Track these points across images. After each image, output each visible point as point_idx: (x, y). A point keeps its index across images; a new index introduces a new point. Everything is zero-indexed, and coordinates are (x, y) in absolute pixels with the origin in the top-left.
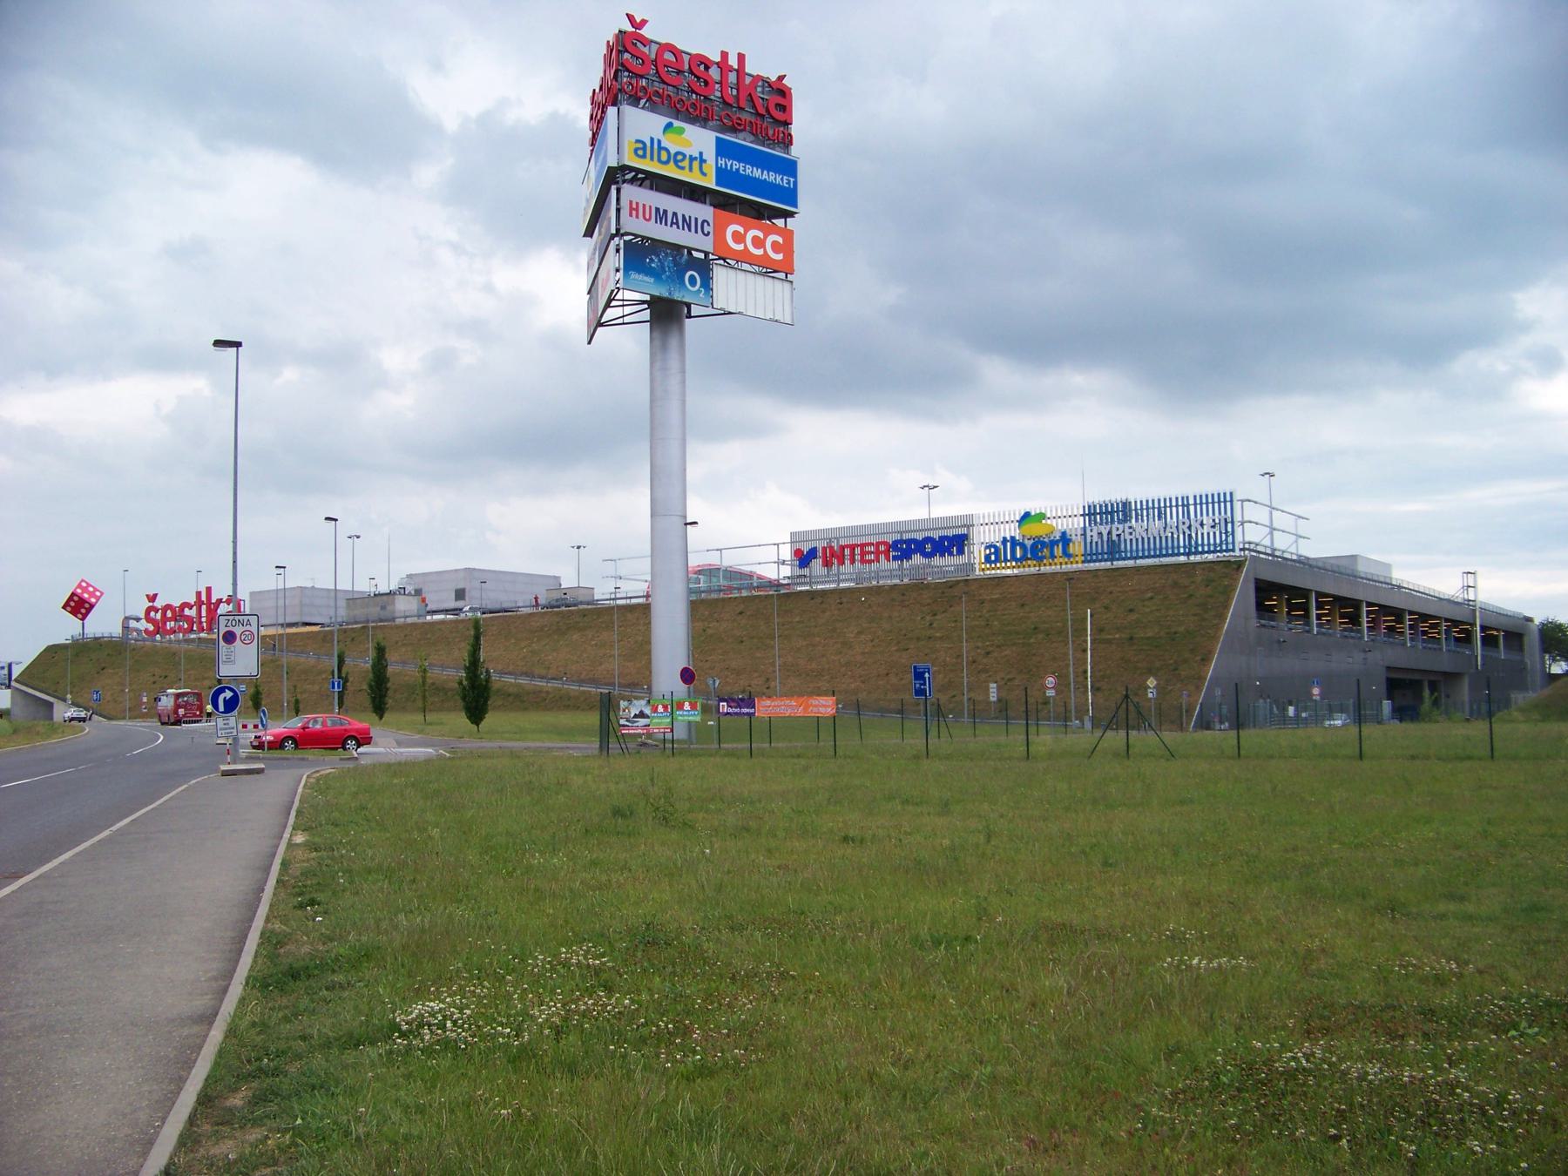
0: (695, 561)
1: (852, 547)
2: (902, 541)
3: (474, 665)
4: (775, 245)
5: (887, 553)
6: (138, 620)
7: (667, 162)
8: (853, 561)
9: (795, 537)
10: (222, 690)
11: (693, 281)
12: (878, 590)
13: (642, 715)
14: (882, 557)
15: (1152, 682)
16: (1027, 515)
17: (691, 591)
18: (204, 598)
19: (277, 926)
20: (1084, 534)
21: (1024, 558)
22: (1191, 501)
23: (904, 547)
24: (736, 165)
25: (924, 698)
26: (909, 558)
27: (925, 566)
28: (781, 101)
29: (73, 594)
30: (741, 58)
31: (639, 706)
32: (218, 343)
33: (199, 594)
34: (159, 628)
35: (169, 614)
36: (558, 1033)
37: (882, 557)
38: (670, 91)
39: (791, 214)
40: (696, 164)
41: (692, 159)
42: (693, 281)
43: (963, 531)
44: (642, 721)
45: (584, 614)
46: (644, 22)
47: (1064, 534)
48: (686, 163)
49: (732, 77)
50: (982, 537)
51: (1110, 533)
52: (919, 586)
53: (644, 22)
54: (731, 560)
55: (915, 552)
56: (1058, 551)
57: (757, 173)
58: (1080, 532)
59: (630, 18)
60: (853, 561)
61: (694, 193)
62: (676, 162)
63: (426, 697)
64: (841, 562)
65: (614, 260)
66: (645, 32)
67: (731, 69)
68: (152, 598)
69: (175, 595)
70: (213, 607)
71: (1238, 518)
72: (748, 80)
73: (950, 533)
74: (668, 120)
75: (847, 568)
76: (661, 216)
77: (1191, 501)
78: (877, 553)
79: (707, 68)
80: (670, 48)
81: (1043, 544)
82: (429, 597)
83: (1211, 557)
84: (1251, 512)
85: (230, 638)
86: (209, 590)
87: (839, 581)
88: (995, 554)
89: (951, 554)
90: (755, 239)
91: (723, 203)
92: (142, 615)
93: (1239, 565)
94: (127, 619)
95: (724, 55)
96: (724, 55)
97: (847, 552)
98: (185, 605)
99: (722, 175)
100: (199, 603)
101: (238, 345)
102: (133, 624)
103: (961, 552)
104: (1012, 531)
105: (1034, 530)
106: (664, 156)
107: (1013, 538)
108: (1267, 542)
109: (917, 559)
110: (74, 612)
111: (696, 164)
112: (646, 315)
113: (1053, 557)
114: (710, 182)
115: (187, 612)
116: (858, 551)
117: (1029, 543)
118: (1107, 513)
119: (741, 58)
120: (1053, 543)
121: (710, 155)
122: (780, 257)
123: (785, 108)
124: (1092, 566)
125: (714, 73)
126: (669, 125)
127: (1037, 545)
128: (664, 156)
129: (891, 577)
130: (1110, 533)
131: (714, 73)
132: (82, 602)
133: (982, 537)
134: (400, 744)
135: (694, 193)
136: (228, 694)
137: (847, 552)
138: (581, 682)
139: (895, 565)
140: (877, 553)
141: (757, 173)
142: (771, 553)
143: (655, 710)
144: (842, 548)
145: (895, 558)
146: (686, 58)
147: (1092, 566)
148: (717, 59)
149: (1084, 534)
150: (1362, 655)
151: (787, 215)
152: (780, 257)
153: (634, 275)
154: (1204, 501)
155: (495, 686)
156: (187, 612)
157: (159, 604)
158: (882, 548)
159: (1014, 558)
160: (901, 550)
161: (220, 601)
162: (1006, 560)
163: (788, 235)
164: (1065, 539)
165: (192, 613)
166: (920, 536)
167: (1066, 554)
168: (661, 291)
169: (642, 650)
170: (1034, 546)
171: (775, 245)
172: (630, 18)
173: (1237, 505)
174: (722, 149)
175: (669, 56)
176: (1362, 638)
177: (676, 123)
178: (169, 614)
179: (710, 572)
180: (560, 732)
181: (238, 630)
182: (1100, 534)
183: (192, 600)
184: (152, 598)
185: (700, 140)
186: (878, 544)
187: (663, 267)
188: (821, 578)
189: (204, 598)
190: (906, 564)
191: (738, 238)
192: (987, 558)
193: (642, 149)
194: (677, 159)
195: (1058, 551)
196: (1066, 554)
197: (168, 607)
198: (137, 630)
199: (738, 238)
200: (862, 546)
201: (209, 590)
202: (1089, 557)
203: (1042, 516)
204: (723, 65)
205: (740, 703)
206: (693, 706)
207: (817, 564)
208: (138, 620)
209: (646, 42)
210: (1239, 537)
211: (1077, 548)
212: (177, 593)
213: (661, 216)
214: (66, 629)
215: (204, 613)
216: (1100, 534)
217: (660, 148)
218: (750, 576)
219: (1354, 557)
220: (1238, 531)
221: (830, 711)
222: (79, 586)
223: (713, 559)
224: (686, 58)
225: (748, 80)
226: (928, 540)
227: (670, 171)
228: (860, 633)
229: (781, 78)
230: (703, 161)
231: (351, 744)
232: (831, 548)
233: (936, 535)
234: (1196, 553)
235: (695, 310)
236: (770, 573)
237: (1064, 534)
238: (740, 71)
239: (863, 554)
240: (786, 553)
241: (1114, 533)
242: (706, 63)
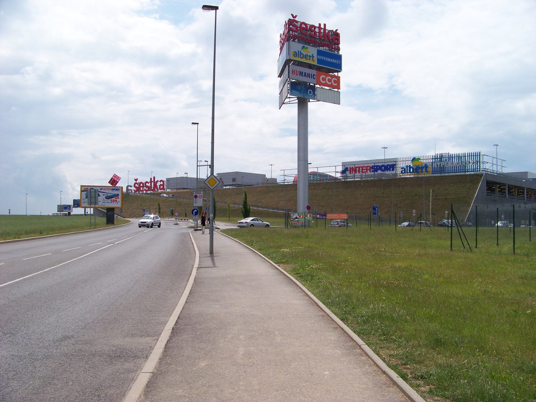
0: (310, 170)
1: (359, 168)
2: (375, 166)
3: (245, 202)
4: (334, 81)
5: (370, 170)
6: (131, 186)
7: (303, 58)
8: (359, 172)
9: (344, 164)
10: (194, 210)
11: (310, 92)
12: (367, 181)
13: (296, 218)
14: (368, 171)
15: (414, 211)
16: (414, 158)
17: (309, 181)
18: (153, 180)
20: (432, 165)
23: (376, 167)
24: (323, 58)
25: (373, 215)
26: (377, 171)
27: (382, 174)
28: (337, 38)
29: (112, 178)
30: (325, 25)
31: (296, 215)
32: (193, 123)
33: (151, 179)
34: (138, 189)
35: (141, 185)
37: (368, 171)
38: (304, 36)
39: (340, 72)
40: (311, 58)
42: (310, 92)
43: (394, 163)
44: (297, 220)
45: (274, 187)
46: (296, 16)
47: (426, 165)
48: (308, 58)
49: (322, 31)
50: (401, 165)
51: (440, 165)
52: (380, 180)
53: (296, 16)
54: (321, 171)
55: (379, 169)
56: (424, 170)
57: (329, 60)
58: (431, 164)
59: (292, 15)
61: (310, 66)
62: (305, 58)
63: (93, 225)
64: (356, 172)
65: (287, 86)
66: (296, 19)
67: (322, 29)
68: (136, 180)
69: (143, 179)
71: (481, 160)
72: (327, 31)
73: (390, 164)
74: (303, 45)
75: (357, 174)
76: (301, 74)
78: (367, 170)
79: (315, 29)
80: (304, 23)
81: (419, 168)
82: (224, 181)
83: (472, 173)
84: (485, 159)
85: (196, 197)
86: (154, 178)
87: (355, 178)
88: (404, 170)
89: (390, 170)
90: (329, 79)
91: (318, 69)
92: (133, 185)
93: (481, 175)
94: (128, 186)
95: (320, 24)
96: (320, 24)
97: (357, 169)
98: (147, 182)
99: (319, 61)
100: (151, 182)
101: (198, 124)
102: (129, 188)
103: (393, 170)
105: (416, 163)
106: (302, 56)
107: (410, 166)
108: (491, 168)
109: (379, 172)
111: (311, 58)
112: (297, 101)
113: (422, 172)
114: (315, 63)
115: (147, 184)
116: (361, 169)
117: (415, 167)
119: (325, 25)
120: (422, 168)
121: (315, 55)
122: (336, 85)
123: (338, 39)
124: (434, 175)
125: (317, 30)
126: (304, 47)
128: (302, 56)
129: (371, 177)
130: (440, 165)
131: (317, 30)
132: (115, 181)
133: (401, 165)
134: (226, 226)
135: (310, 66)
136: (196, 211)
137: (357, 169)
138: (273, 209)
139: (373, 173)
140: (367, 170)
141: (329, 60)
142: (333, 169)
143: (300, 216)
144: (356, 168)
145: (372, 171)
146: (308, 26)
147: (434, 175)
148: (318, 26)
149: (432, 165)
150: (524, 205)
151: (338, 72)
152: (336, 85)
153: (293, 91)
155: (251, 211)
156: (147, 184)
158: (368, 168)
159: (410, 172)
160: (374, 169)
161: (158, 181)
163: (338, 78)
164: (426, 166)
165: (149, 185)
166: (380, 165)
168: (301, 96)
169: (294, 200)
171: (334, 81)
172: (292, 15)
173: (481, 157)
174: (319, 53)
175: (303, 26)
176: (524, 200)
177: (306, 46)
178: (141, 185)
179: (314, 174)
181: (198, 195)
182: (437, 165)
183: (149, 181)
185: (312, 51)
186: (367, 167)
187: (301, 89)
188: (351, 178)
189: (153, 180)
190: (376, 173)
191: (324, 79)
192: (402, 172)
193: (295, 54)
194: (306, 57)
195: (424, 170)
196: (426, 171)
197: (141, 183)
198: (131, 190)
199: (324, 79)
200: (362, 167)
201: (154, 178)
202: (434, 172)
203: (419, 159)
204: (320, 27)
205: (323, 215)
206: (310, 216)
207: (348, 172)
208: (131, 186)
209: (297, 22)
210: (482, 167)
211: (430, 169)
212: (144, 179)
213: (301, 74)
216: (437, 165)
217: (301, 54)
218: (327, 175)
219: (526, 173)
220: (482, 165)
221: (346, 218)
223: (315, 170)
224: (308, 26)
225: (327, 31)
226: (383, 166)
227: (304, 60)
228: (361, 195)
229: (337, 30)
230: (313, 57)
233: (386, 164)
234: (468, 172)
235: (311, 100)
236: (333, 175)
237: (426, 165)
238: (325, 29)
239: (362, 170)
240: (340, 169)
241: (442, 165)
242: (315, 27)
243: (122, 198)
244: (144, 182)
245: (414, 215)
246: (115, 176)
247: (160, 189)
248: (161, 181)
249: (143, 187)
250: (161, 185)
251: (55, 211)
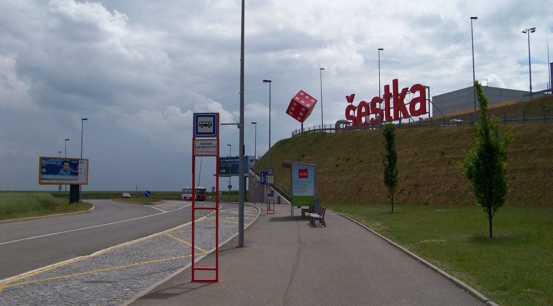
18: (391, 91)
19: (297, 98)
29: (293, 101)
33: (387, 87)
35: (363, 110)
68: (350, 99)
70: (399, 98)
86: (395, 82)
98: (376, 100)
100: (387, 95)
110: (295, 116)
132: (300, 106)
157: (356, 103)
161: (405, 91)
180: (22, 221)
184: (350, 99)
189: (391, 91)
197: (363, 104)
201: (395, 82)
214: (289, 127)
215: (392, 105)
222: (298, 95)
229: (214, 175)
231: (188, 198)
243: (264, 200)
244: (369, 101)
245: (428, 241)
246: (302, 95)
247: (415, 113)
248: (415, 88)
249: (367, 114)
250: (413, 103)
251: (329, 214)
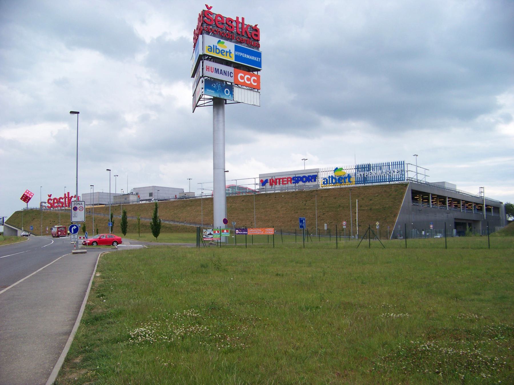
0: (228, 184)
1: (279, 179)
2: (296, 177)
3: (155, 218)
4: (254, 80)
5: (291, 181)
6: (45, 203)
7: (219, 53)
8: (279, 184)
9: (261, 176)
10: (73, 226)
11: (227, 92)
12: (288, 193)
13: (210, 234)
14: (289, 182)
15: (377, 223)
16: (337, 169)
17: (226, 194)
18: (67, 196)
19: (91, 303)
20: (355, 175)
21: (336, 183)
22: (391, 164)
23: (296, 179)
24: (241, 54)
25: (303, 229)
26: (298, 183)
27: (303, 185)
28: (256, 33)
29: (24, 194)
30: (243, 19)
31: (209, 231)
32: (71, 112)
33: (65, 194)
34: (52, 206)
35: (55, 201)
36: (183, 338)
37: (289, 182)
38: (220, 30)
39: (259, 70)
40: (228, 54)
41: (227, 52)
42: (227, 92)
43: (316, 174)
44: (211, 236)
45: (191, 201)
46: (211, 7)
47: (349, 175)
48: (225, 54)
49: (240, 25)
50: (322, 176)
51: (364, 174)
52: (301, 192)
53: (211, 7)
54: (240, 183)
55: (300, 181)
56: (347, 180)
57: (248, 57)
58: (354, 174)
59: (207, 6)
60: (279, 184)
61: (228, 63)
62: (222, 53)
63: (140, 228)
64: (276, 184)
65: (201, 85)
66: (211, 10)
67: (240, 23)
68: (50, 196)
69: (57, 195)
70: (70, 199)
71: (406, 169)
72: (245, 26)
73: (311, 174)
74: (219, 39)
75: (278, 186)
76: (217, 71)
77: (391, 164)
78: (288, 181)
79: (232, 22)
80: (220, 16)
81: (342, 178)
82: (141, 196)
83: (397, 182)
84: (410, 168)
85: (75, 209)
86: (68, 193)
87: (275, 190)
88: (326, 181)
89: (312, 181)
90: (247, 78)
91: (237, 66)
92: (47, 201)
93: (406, 185)
94: (42, 203)
95: (237, 18)
96: (237, 18)
97: (278, 181)
98: (61, 198)
99: (237, 57)
100: (65, 197)
101: (78, 113)
102: (44, 204)
103: (315, 181)
104: (332, 174)
105: (339, 173)
106: (218, 51)
107: (332, 176)
108: (415, 177)
109: (301, 183)
110: (24, 200)
111: (228, 54)
112: (212, 103)
113: (345, 182)
114: (233, 60)
115: (61, 200)
116: (281, 180)
117: (337, 178)
118: (363, 168)
119: (243, 19)
120: (345, 178)
121: (233, 51)
122: (256, 84)
123: (257, 35)
124: (358, 185)
125: (234, 24)
126: (219, 41)
127: (340, 178)
128: (218, 51)
129: (292, 189)
130: (364, 174)
131: (234, 24)
132: (27, 197)
133: (322, 176)
134: (131, 244)
135: (228, 63)
136: (75, 227)
137: (278, 181)
138: (191, 223)
139: (293, 185)
140: (288, 181)
141: (248, 57)
142: (253, 181)
143: (215, 232)
144: (276, 179)
145: (293, 183)
146: (225, 19)
147: (358, 185)
148: (235, 19)
149: (355, 175)
150: (447, 215)
151: (258, 70)
152: (256, 84)
153: (208, 90)
154: (395, 164)
155: (162, 225)
156: (61, 200)
157: (52, 198)
158: (289, 179)
159: (332, 183)
160: (295, 180)
161: (72, 197)
162: (330, 183)
163: (258, 77)
164: (349, 177)
165: (63, 201)
166: (301, 176)
167: (349, 181)
168: (217, 95)
169: (210, 213)
170: (339, 179)
171: (254, 80)
172: (207, 6)
173: (406, 165)
174: (237, 49)
175: (219, 18)
176: (446, 209)
177: (222, 40)
178: (55, 201)
179: (233, 187)
180: (184, 240)
181: (78, 206)
182: (361, 175)
183: (63, 196)
184: (50, 196)
185: (229, 46)
186: (288, 178)
187: (217, 88)
188: (269, 189)
189: (67, 196)
190: (297, 185)
191: (242, 78)
192: (324, 183)
193: (210, 49)
194: (222, 52)
195: (347, 180)
196: (349, 181)
197: (55, 199)
198: (45, 206)
199: (242, 78)
200: (283, 179)
201: (68, 193)
202: (357, 182)
203: (342, 169)
204: (237, 21)
205: (243, 230)
206: (227, 231)
207: (268, 185)
208: (45, 203)
209: (212, 14)
210: (406, 176)
211: (353, 179)
212: (58, 194)
213: (217, 71)
214: (22, 206)
215: (67, 201)
216: (361, 175)
217: (216, 49)
218: (246, 188)
219: (444, 183)
220: (406, 174)
221: (272, 233)
222: (26, 192)
223: (234, 183)
224: (225, 19)
225: (245, 26)
226: (304, 177)
227: (220, 56)
228: (282, 207)
229: (256, 26)
230: (230, 53)
231: (115, 243)
232: (273, 179)
233: (307, 175)
234: (392, 181)
235: (228, 102)
236: (253, 187)
237: (349, 175)
238: (243, 23)
239: (283, 181)
240: (258, 181)
241: (365, 174)
242: (231, 21)
